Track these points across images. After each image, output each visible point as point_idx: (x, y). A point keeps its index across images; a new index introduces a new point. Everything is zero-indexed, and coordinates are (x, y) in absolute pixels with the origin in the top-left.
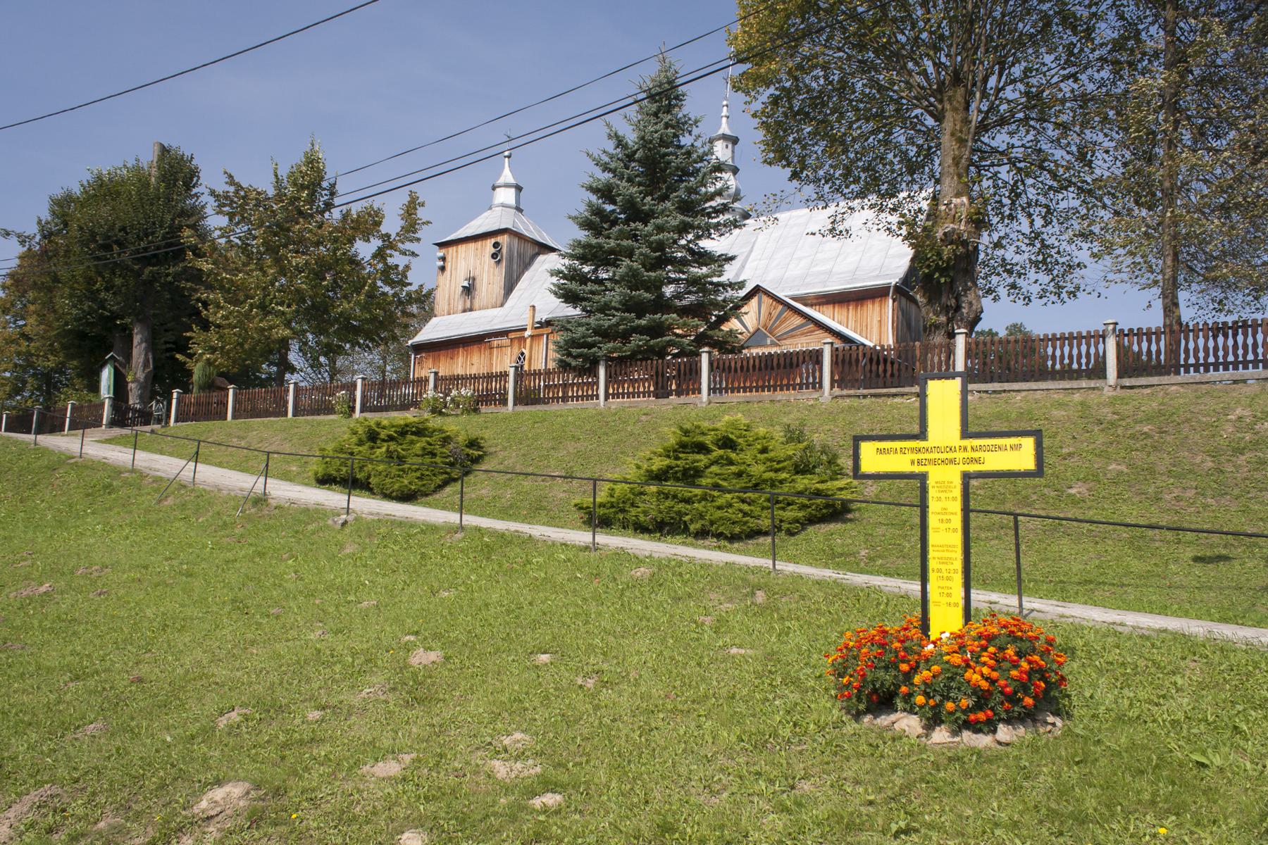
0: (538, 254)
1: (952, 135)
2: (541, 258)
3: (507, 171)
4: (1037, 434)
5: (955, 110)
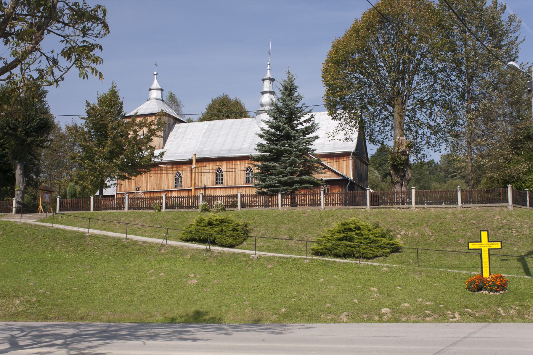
0: (175, 123)
1: (398, 114)
2: (177, 125)
3: (156, 82)
4: (501, 242)
5: (398, 105)
